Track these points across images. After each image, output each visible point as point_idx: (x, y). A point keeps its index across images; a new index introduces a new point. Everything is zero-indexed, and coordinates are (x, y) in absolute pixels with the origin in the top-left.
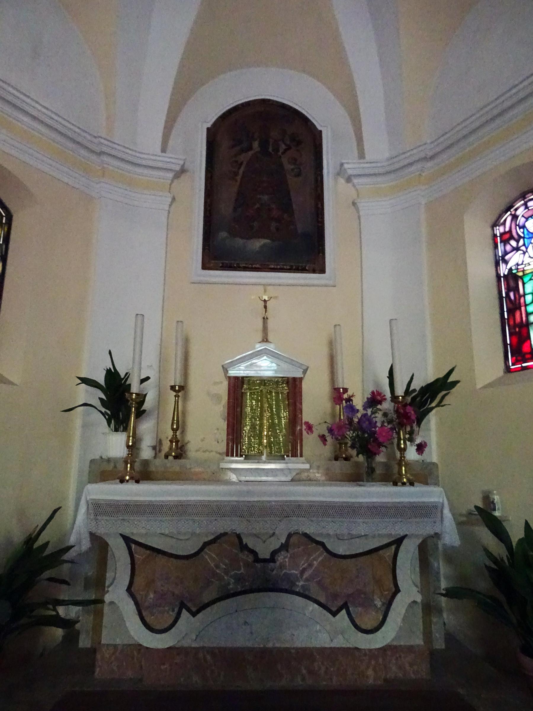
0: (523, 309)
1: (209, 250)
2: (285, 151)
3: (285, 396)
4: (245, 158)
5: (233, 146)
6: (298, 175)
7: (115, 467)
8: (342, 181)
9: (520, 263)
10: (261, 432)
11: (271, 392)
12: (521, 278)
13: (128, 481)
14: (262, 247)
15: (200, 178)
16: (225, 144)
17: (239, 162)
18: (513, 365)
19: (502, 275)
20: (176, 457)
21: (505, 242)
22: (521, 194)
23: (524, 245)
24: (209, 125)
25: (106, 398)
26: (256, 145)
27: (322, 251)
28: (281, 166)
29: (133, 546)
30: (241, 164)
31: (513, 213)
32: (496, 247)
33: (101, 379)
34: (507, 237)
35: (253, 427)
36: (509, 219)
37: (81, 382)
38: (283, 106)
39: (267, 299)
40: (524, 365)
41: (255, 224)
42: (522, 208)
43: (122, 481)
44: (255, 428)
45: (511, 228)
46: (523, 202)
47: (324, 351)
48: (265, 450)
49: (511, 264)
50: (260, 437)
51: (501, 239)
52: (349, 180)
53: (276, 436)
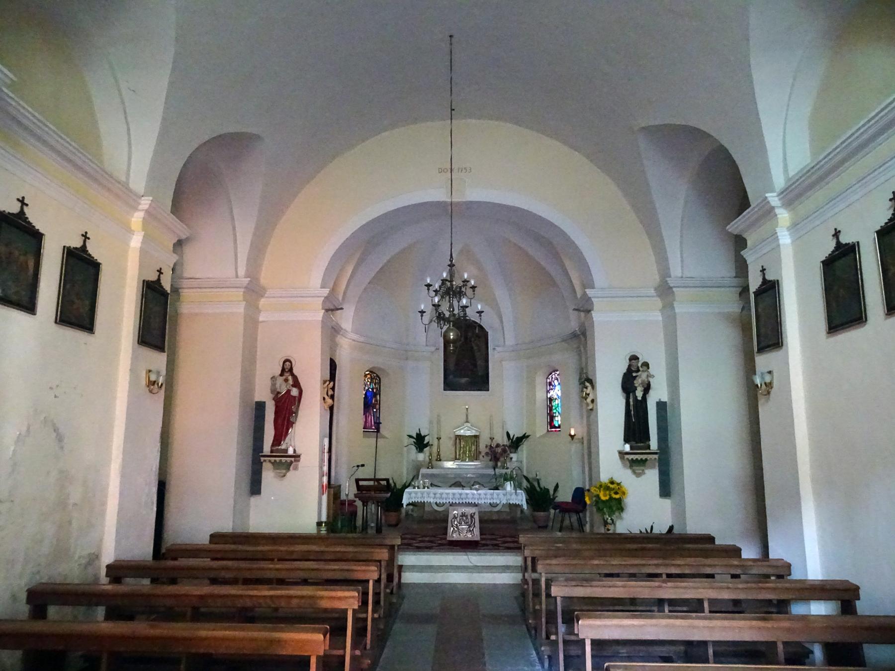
36: (551, 378)
37: (415, 437)
43: (428, 468)
53: (471, 454)
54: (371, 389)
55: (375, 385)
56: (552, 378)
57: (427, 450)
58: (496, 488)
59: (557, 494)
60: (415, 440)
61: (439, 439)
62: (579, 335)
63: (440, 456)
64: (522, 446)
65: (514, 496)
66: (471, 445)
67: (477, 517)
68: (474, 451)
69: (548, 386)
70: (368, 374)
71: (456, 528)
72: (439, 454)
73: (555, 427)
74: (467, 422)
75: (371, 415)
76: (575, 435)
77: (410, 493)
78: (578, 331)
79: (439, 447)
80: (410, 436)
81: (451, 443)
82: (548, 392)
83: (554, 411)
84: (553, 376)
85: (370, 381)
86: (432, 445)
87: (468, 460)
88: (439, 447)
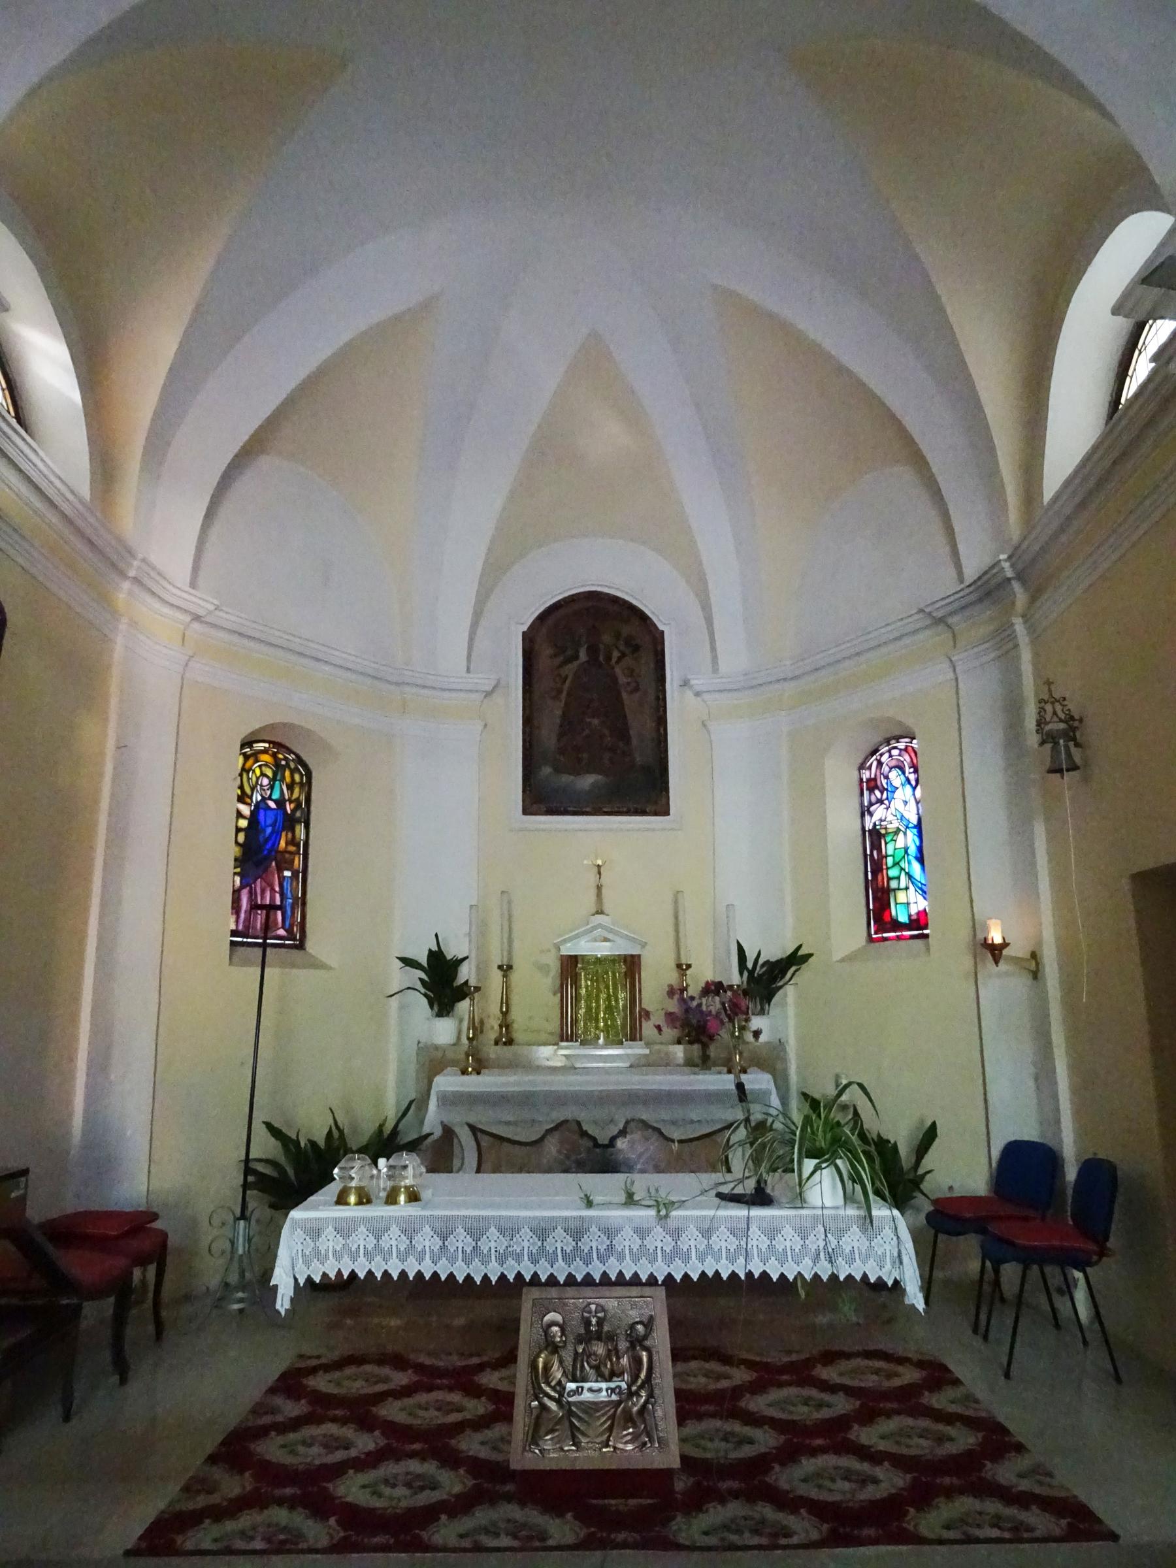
0: (885, 871)
1: (530, 791)
2: (619, 660)
3: (622, 975)
4: (570, 669)
5: (555, 655)
6: (637, 689)
7: (444, 1055)
8: (689, 694)
9: (883, 818)
10: (597, 1014)
11: (607, 973)
12: (884, 836)
13: (471, 1073)
14: (594, 785)
15: (516, 689)
16: (545, 652)
17: (563, 676)
18: (876, 933)
19: (867, 829)
20: (505, 1044)
21: (871, 790)
22: (885, 739)
23: (887, 799)
24: (525, 628)
25: (429, 977)
26: (583, 656)
27: (665, 788)
28: (615, 679)
29: (479, 1135)
30: (566, 677)
31: (878, 758)
32: (862, 794)
33: (423, 960)
34: (873, 785)
35: (589, 1008)
36: (875, 764)
37: (425, 964)
38: (615, 600)
39: (600, 864)
40: (885, 935)
41: (585, 755)
42: (887, 755)
43: (464, 1072)
44: (591, 1010)
45: (876, 775)
46: (887, 748)
47: (669, 908)
48: (602, 1034)
49: (876, 818)
50: (597, 1021)
51: (867, 785)
52: (697, 694)
53: (614, 1020)
54: (275, 801)
55: (290, 787)
56: (880, 764)
57: (463, 1006)
58: (761, 1198)
59: (928, 1162)
60: (424, 976)
61: (506, 969)
62: (1009, 579)
63: (507, 1027)
64: (780, 993)
65: (854, 1239)
66: (615, 988)
67: (661, 1340)
68: (625, 1006)
69: (866, 793)
70: (265, 751)
71: (558, 1401)
72: (506, 1024)
73: (896, 925)
74: (600, 912)
75: (273, 890)
76: (1005, 945)
77: (314, 1232)
78: (1006, 565)
79: (506, 1001)
80: (408, 962)
81: (548, 982)
82: (865, 811)
83: (893, 873)
84: (885, 758)
85: (269, 773)
86: (477, 989)
87: (606, 1038)
88: (506, 1001)
